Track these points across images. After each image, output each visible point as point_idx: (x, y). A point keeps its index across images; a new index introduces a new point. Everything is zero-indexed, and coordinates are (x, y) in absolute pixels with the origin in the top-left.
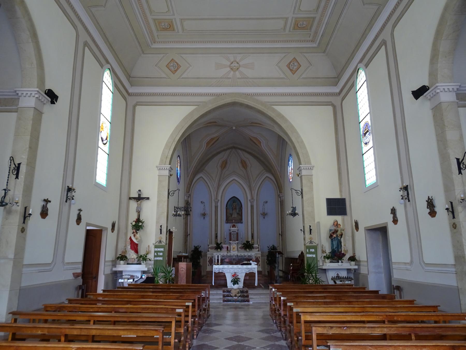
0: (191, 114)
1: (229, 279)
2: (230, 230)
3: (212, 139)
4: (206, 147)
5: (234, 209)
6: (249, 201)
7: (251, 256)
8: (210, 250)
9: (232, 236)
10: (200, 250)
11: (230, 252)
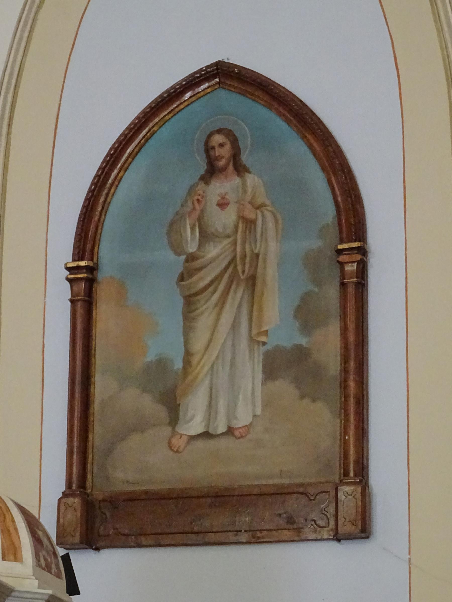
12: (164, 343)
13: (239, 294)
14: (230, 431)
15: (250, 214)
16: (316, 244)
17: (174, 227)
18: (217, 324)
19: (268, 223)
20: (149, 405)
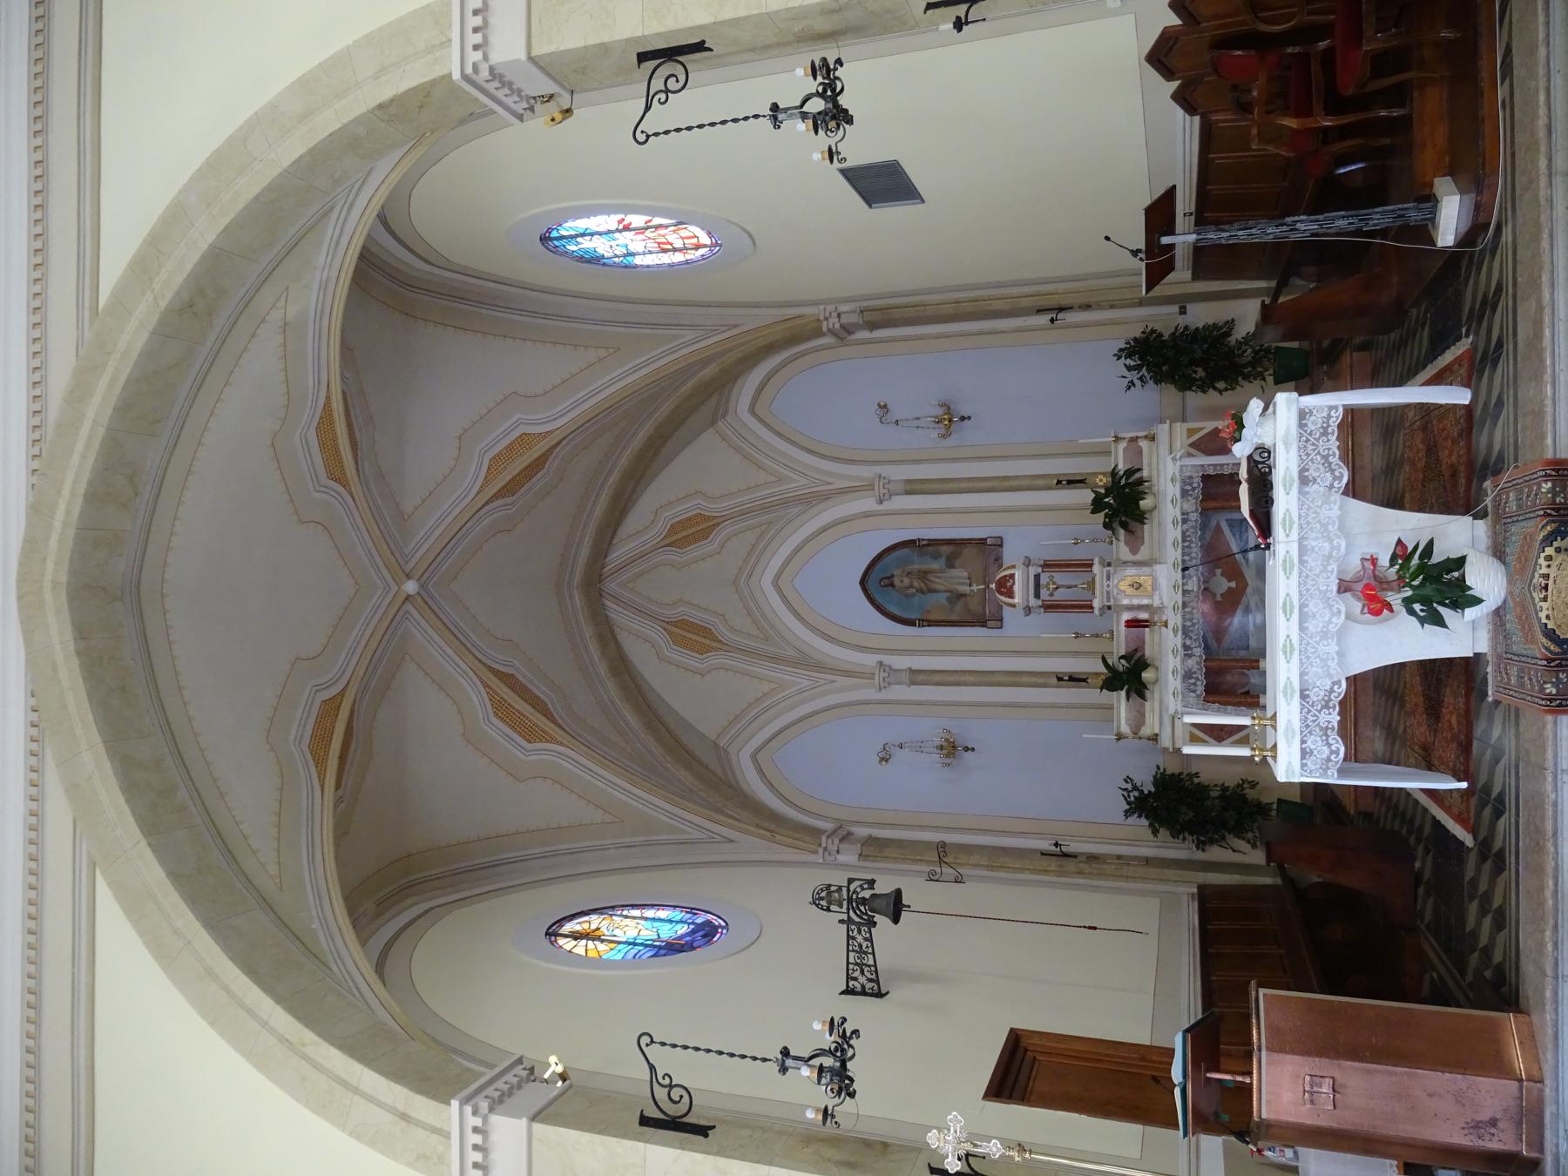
0: (134, 905)
1: (1406, 640)
2: (1028, 610)
3: (501, 709)
4: (553, 740)
5: (924, 582)
6: (886, 506)
7: (1186, 481)
8: (1146, 731)
9: (1060, 595)
10: (1149, 787)
11: (1161, 609)
12: (942, 598)
17: (907, 596)
18: (939, 583)
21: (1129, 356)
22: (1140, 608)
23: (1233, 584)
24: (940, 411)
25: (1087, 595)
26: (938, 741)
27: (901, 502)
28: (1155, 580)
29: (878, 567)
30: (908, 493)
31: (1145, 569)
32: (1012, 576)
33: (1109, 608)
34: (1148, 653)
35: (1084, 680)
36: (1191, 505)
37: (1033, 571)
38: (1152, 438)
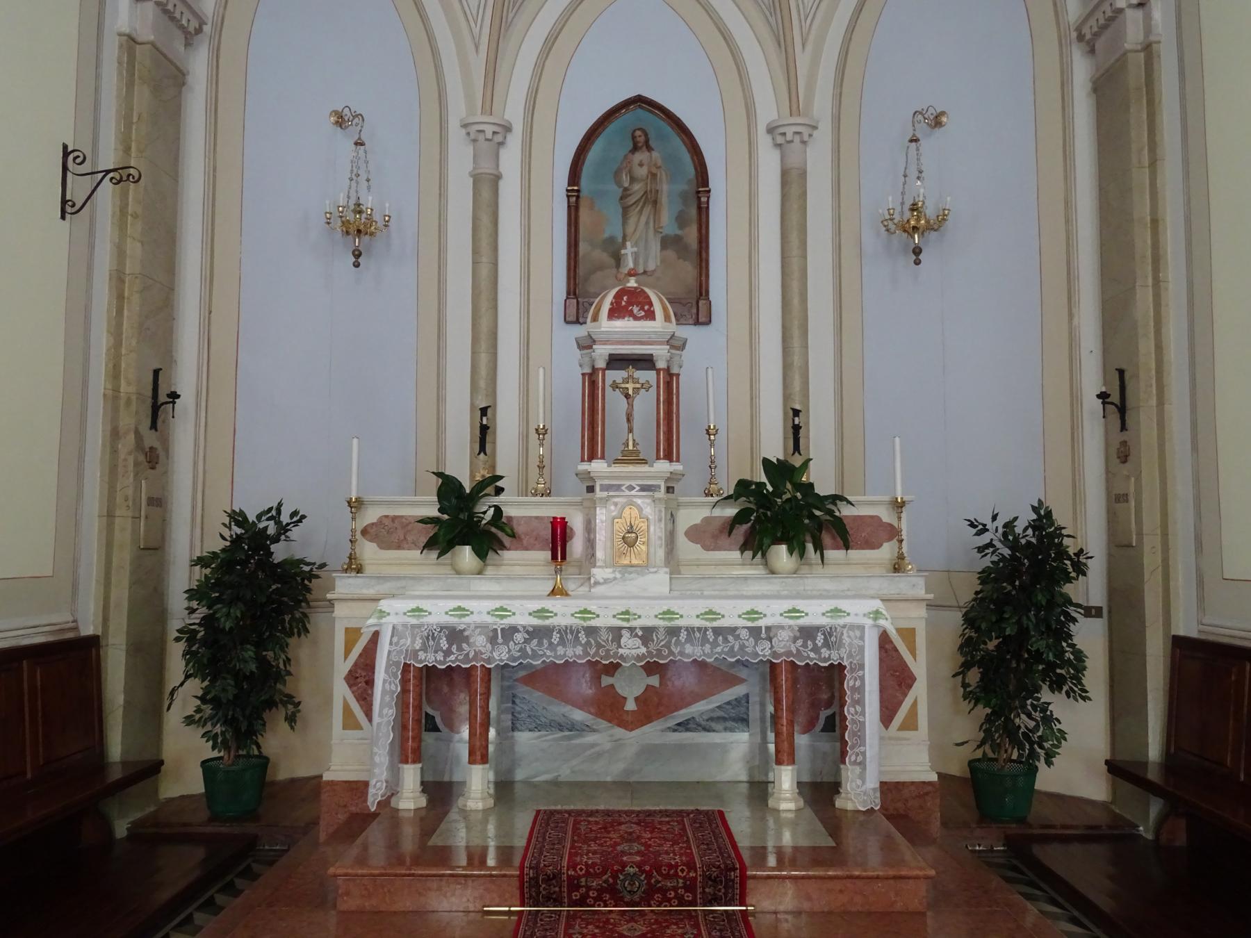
6: (764, 142)
7: (830, 635)
8: (369, 551)
9: (614, 404)
12: (613, 228)
13: (648, 209)
14: (645, 272)
15: (654, 170)
16: (686, 187)
17: (617, 174)
18: (639, 221)
19: (662, 175)
20: (605, 258)
21: (1036, 526)
22: (590, 543)
23: (631, 706)
24: (930, 211)
25: (614, 450)
26: (368, 201)
27: (769, 164)
28: (644, 568)
29: (668, 129)
30: (785, 174)
31: (661, 553)
32: (650, 315)
33: (591, 489)
34: (507, 555)
35: (482, 449)
36: (783, 643)
37: (661, 353)
38: (897, 567)
